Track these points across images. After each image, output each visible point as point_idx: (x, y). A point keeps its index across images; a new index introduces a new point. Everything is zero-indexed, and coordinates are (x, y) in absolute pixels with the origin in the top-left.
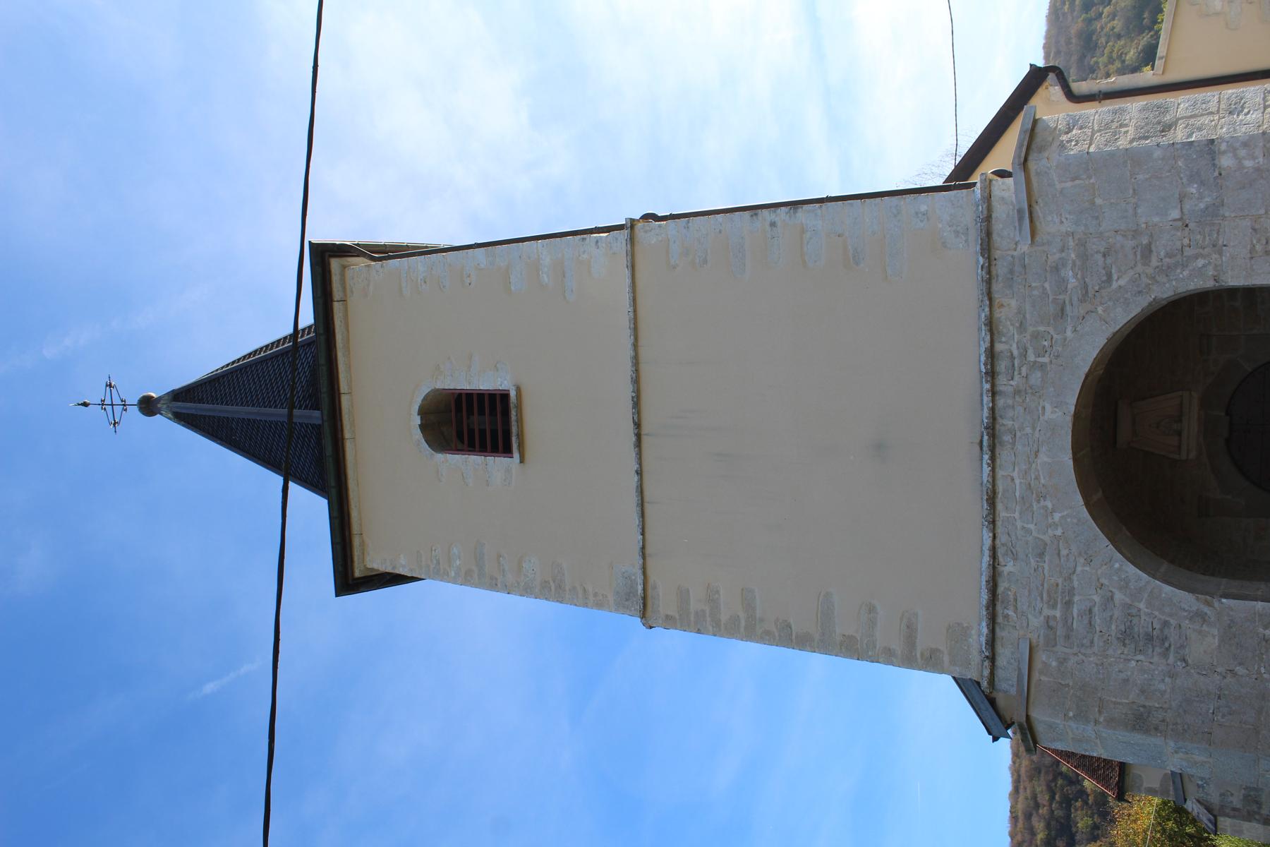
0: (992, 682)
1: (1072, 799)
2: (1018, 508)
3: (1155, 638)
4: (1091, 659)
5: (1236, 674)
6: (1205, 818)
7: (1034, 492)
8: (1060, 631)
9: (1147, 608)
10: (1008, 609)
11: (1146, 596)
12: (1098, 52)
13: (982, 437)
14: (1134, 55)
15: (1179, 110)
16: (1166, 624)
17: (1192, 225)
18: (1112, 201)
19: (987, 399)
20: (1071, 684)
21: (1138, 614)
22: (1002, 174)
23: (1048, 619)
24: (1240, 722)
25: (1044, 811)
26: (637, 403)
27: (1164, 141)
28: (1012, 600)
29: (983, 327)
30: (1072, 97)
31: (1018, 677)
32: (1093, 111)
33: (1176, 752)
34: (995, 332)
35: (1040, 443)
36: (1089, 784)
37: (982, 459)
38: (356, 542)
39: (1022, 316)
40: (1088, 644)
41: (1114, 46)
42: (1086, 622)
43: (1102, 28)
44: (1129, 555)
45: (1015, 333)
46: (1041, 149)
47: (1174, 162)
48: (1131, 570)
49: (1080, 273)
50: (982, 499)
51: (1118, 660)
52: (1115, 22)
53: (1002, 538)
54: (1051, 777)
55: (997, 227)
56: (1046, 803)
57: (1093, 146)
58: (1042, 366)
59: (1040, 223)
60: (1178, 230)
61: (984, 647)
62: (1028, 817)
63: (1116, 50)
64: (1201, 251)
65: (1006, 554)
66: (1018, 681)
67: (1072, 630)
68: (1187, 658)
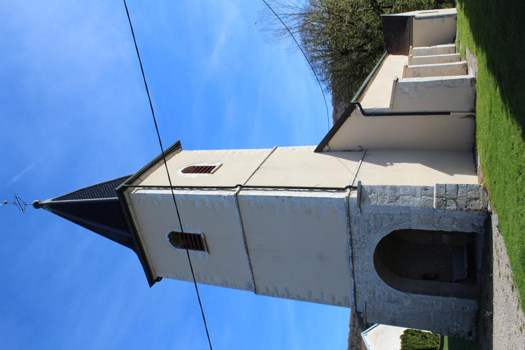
2: (360, 273)
8: (372, 299)
26: (245, 243)
38: (152, 271)
46: (364, 201)
53: (356, 279)
55: (351, 209)
60: (400, 215)
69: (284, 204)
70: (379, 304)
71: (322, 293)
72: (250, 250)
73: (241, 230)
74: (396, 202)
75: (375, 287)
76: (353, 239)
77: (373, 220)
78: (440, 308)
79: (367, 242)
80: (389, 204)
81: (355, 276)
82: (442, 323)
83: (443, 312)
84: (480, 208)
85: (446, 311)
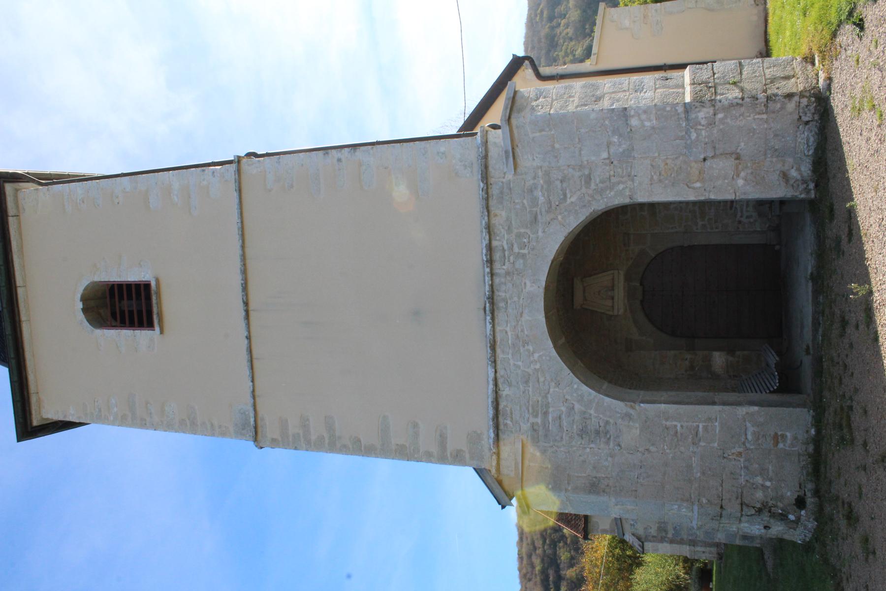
2: (511, 351)
3: (601, 432)
4: (562, 449)
6: (636, 544)
7: (521, 341)
9: (596, 413)
10: (507, 420)
11: (594, 405)
12: (558, 49)
13: (485, 304)
14: (580, 51)
15: (605, 88)
16: (607, 423)
17: (615, 162)
19: (487, 279)
22: (494, 127)
23: (533, 424)
25: (539, 551)
26: (245, 288)
27: (597, 107)
28: (509, 414)
29: (484, 230)
32: (552, 86)
33: (616, 505)
34: (492, 233)
37: (486, 319)
38: (33, 400)
40: (559, 440)
41: (568, 45)
42: (557, 425)
43: (561, 33)
46: (520, 111)
48: (585, 388)
49: (546, 194)
50: (487, 346)
52: (569, 30)
53: (501, 372)
55: (492, 162)
56: (541, 546)
59: (520, 160)
60: (607, 166)
62: (530, 556)
63: (569, 47)
64: (621, 179)
65: (504, 383)
66: (515, 467)
69: (340, 170)
70: (557, 446)
71: (415, 426)
72: (252, 310)
73: (239, 252)
74: (596, 104)
75: (549, 392)
76: (497, 247)
77: (542, 187)
78: (716, 445)
79: (529, 253)
80: (579, 109)
81: (498, 362)
82: (722, 481)
83: (726, 455)
84: (800, 90)
85: (733, 451)
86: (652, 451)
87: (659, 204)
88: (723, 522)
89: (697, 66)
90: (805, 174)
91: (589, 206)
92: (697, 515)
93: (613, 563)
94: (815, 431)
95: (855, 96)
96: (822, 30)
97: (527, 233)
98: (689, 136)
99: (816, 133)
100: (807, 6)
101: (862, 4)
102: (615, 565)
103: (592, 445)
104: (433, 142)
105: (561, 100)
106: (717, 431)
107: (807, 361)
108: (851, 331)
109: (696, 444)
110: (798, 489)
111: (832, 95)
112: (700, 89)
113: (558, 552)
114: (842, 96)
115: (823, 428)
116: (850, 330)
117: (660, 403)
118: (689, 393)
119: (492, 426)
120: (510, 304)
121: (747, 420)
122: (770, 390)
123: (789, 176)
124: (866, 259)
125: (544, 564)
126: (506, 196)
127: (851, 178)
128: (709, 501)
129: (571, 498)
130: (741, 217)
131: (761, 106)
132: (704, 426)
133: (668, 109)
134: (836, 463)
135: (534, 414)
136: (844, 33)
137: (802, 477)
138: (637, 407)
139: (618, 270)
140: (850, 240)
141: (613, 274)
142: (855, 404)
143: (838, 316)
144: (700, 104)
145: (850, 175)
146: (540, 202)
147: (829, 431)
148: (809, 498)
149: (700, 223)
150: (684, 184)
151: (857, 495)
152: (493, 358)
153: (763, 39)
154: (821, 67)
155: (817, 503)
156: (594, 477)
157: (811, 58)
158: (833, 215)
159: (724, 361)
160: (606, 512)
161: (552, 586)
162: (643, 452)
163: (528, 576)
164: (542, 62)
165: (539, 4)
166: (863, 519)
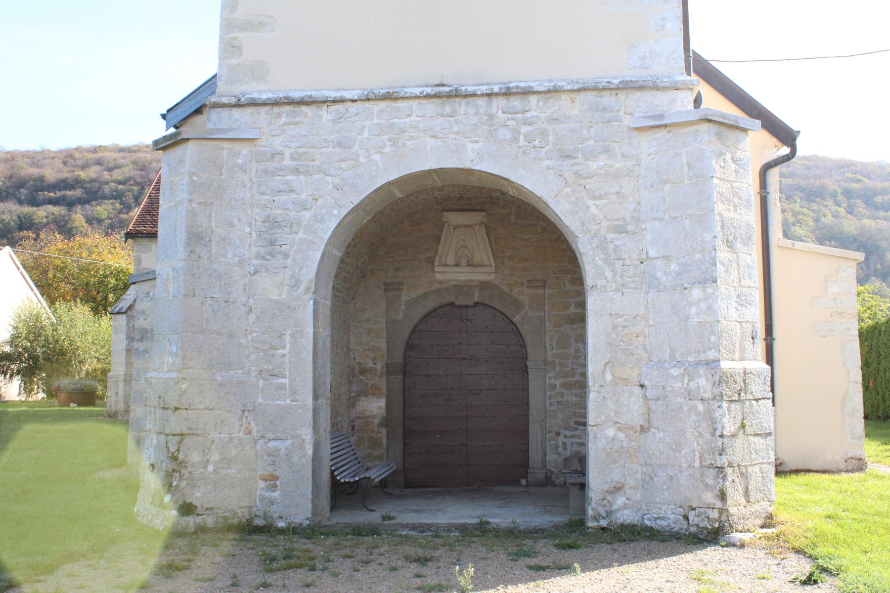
0: (216, 105)
1: (121, 200)
2: (382, 121)
3: (273, 247)
4: (248, 194)
5: (248, 314)
6: (123, 304)
7: (398, 136)
8: (270, 166)
9: (299, 239)
10: (286, 116)
11: (310, 238)
12: (805, 203)
13: (448, 86)
14: (799, 233)
15: (745, 255)
16: (286, 256)
17: (642, 267)
18: (667, 199)
19: (484, 89)
20: (223, 177)
21: (293, 232)
22: (697, 102)
23: (281, 153)
24: (207, 319)
25: (106, 176)
27: (718, 242)
28: (295, 120)
29: (552, 84)
30: (766, 168)
31: (223, 129)
32: (751, 182)
33: (173, 269)
34: (548, 95)
35: (444, 139)
36: (136, 212)
37: (427, 86)
39: (563, 120)
40: (261, 191)
41: (809, 216)
42: (282, 188)
43: (826, 206)
44: (345, 223)
45: (547, 114)
46: (719, 135)
47: (699, 250)
48: (333, 224)
49: (602, 171)
50: (389, 88)
51: (250, 217)
52: (830, 218)
53: (353, 108)
54: (139, 180)
55: (648, 95)
56: (114, 178)
57: (719, 181)
58: (516, 140)
59: (650, 136)
60: (638, 255)
61: (250, 96)
62: (99, 163)
63: (805, 218)
64: (619, 275)
65: (338, 112)
66: (220, 129)
67: (273, 176)
68: (258, 274)
70: (251, 188)
77: (611, 166)
78: (260, 400)
79: (520, 147)
80: (718, 218)
83: (246, 413)
84: (730, 509)
85: (253, 423)
86: (250, 317)
87: (584, 328)
88: (157, 411)
89: (770, 379)
90: (619, 515)
91: (583, 230)
92: (165, 377)
93: (95, 276)
94: (281, 527)
95: (717, 574)
96: (806, 537)
97: (547, 145)
98: (675, 366)
99: (672, 529)
100: (840, 519)
101: (835, 583)
102: (92, 280)
103: (254, 236)
104: (679, 12)
105: (731, 195)
106: (277, 402)
107: (374, 517)
108: (413, 569)
109: (260, 375)
110: (205, 506)
111: (720, 548)
112: (738, 381)
113: (106, 201)
114: (719, 559)
115: (287, 537)
116: (414, 568)
117: (315, 327)
118: (328, 365)
119: (277, 96)
120: (449, 121)
121: (294, 440)
122: (334, 471)
123: (617, 494)
124: (506, 586)
125: (89, 182)
126: (600, 116)
127: (612, 569)
128: (184, 392)
129: (180, 207)
130: (565, 436)
131: (711, 459)
132: (285, 385)
133: (713, 338)
134: (240, 552)
135: (296, 155)
136: (801, 562)
137: (221, 511)
138: (308, 296)
139: (496, 273)
140: (531, 568)
141: (491, 266)
142: (318, 573)
143: (433, 554)
144: (718, 381)
145: (616, 568)
146: (590, 163)
147: (282, 544)
148: (194, 520)
149: (557, 383)
150: (611, 358)
151: (200, 576)
152: (373, 97)
153: (800, 468)
154: (758, 536)
155: (187, 529)
156: (210, 238)
157: (771, 523)
158: (564, 549)
159: (373, 413)
160: (163, 256)
161: (59, 194)
162: (247, 305)
163: (71, 161)
164: (787, 180)
165: (869, 178)
166: (169, 583)
